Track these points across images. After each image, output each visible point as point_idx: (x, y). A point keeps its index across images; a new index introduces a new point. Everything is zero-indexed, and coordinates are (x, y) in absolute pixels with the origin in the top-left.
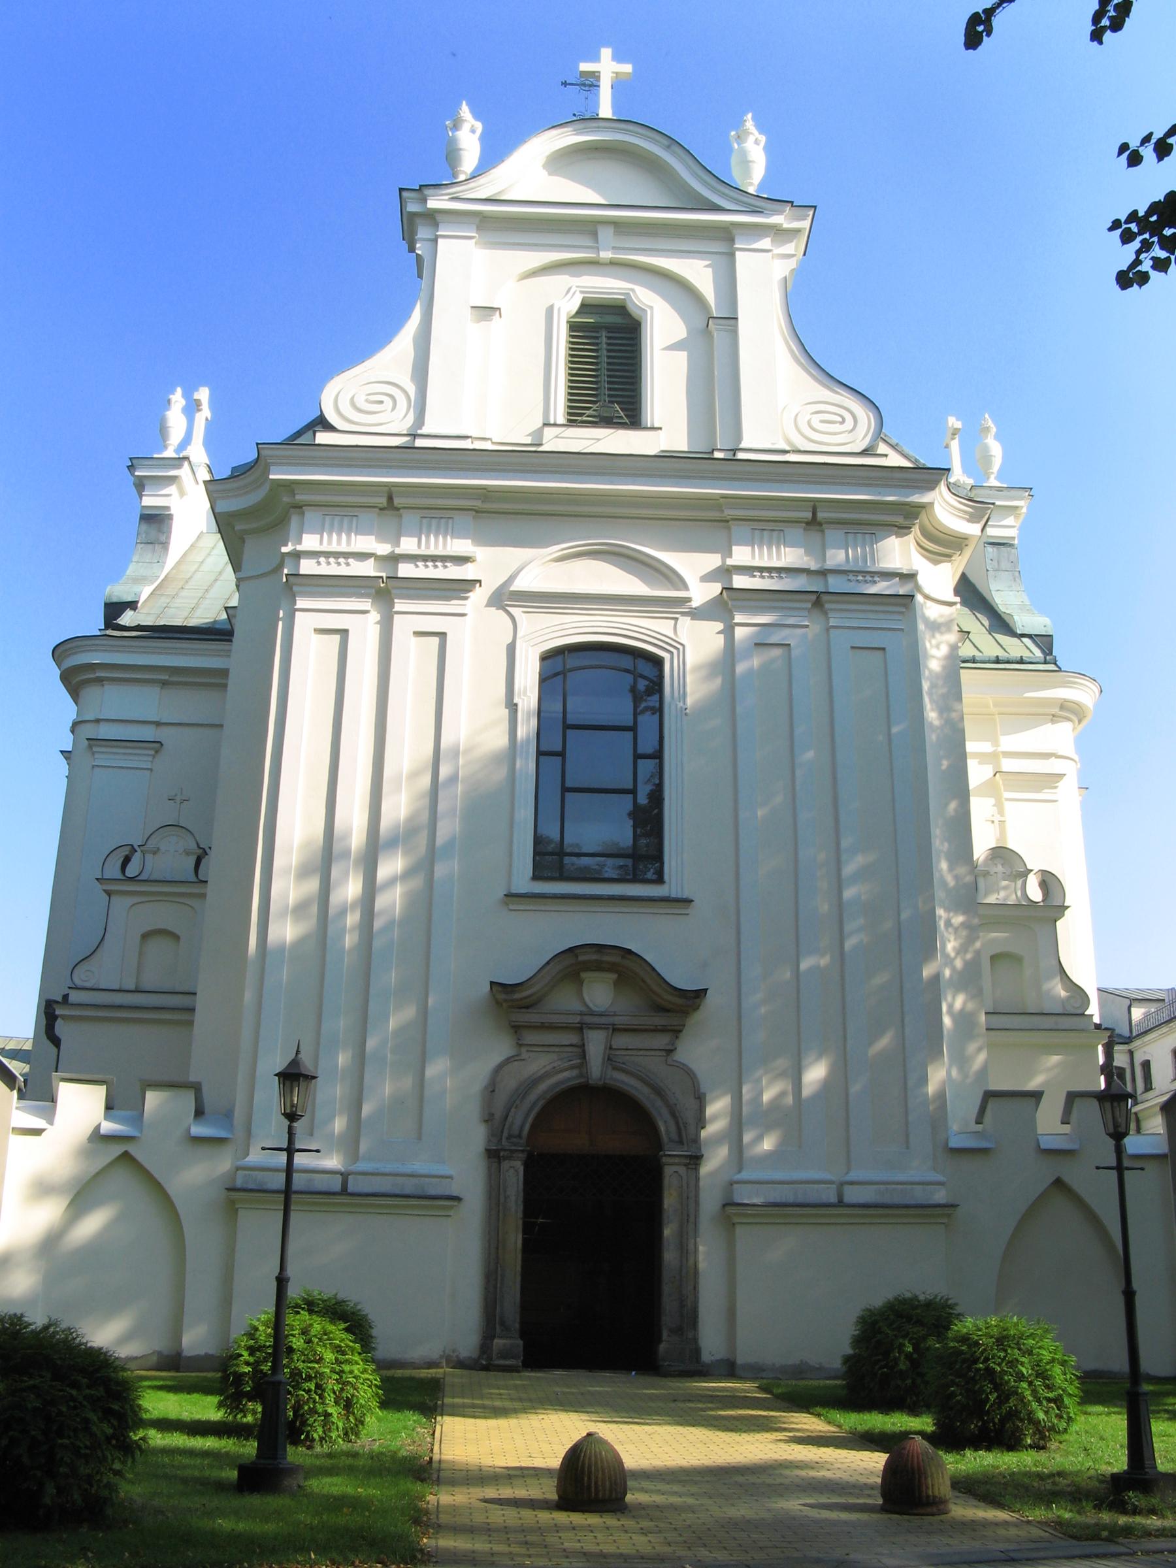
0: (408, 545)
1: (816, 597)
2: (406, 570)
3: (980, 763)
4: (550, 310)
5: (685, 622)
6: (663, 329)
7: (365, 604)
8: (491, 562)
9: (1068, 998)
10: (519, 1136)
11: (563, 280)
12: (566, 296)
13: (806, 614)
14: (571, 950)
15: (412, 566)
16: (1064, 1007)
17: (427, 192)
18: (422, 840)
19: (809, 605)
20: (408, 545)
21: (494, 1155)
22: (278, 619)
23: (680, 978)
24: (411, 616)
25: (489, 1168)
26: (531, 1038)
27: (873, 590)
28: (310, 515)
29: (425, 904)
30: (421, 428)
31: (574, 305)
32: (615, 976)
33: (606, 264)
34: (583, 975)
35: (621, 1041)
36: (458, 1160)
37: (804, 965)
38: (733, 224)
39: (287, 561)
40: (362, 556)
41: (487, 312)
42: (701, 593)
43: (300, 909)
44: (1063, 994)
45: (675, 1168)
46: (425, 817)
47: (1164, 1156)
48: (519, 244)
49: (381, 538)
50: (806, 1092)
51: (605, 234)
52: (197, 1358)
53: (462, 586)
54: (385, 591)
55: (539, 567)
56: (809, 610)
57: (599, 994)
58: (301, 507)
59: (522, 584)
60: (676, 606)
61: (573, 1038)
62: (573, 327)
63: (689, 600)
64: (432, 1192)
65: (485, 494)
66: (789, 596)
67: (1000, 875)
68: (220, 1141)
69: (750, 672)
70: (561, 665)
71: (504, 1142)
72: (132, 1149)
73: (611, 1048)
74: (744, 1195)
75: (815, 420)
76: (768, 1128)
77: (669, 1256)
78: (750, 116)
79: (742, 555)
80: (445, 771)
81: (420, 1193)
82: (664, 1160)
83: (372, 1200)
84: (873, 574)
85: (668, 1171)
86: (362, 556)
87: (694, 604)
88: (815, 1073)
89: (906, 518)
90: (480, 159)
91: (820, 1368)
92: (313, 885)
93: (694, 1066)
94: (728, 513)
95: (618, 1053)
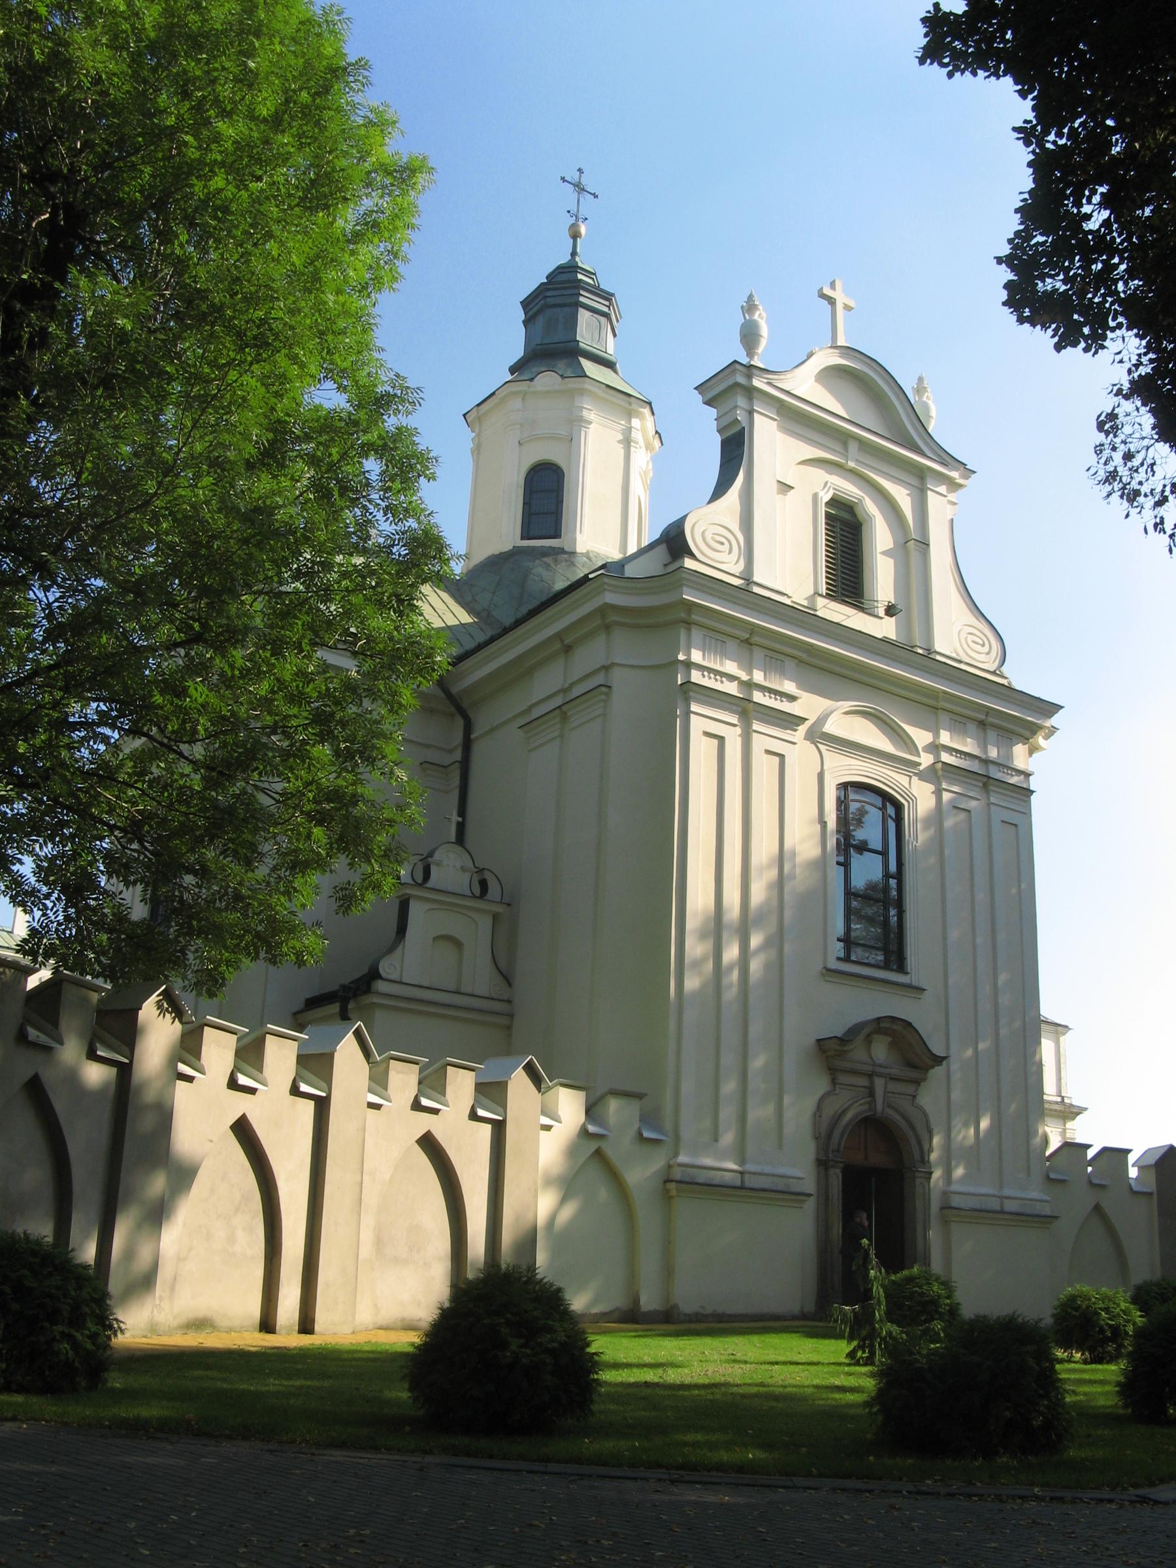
0: (758, 676)
2: (758, 697)
4: (815, 497)
6: (880, 537)
10: (838, 1150)
11: (819, 475)
15: (761, 694)
17: (755, 371)
18: (774, 920)
22: (676, 716)
24: (765, 737)
25: (819, 1173)
26: (844, 1079)
29: (777, 968)
32: (890, 1039)
36: (798, 1166)
38: (929, 468)
39: (681, 668)
41: (785, 487)
46: (775, 903)
47: (1151, 1194)
49: (740, 667)
51: (853, 447)
53: (796, 721)
55: (844, 720)
59: (830, 727)
61: (864, 1081)
65: (810, 649)
66: (970, 775)
71: (831, 1155)
74: (956, 1201)
75: (970, 638)
80: (787, 868)
83: (763, 1194)
94: (942, 704)
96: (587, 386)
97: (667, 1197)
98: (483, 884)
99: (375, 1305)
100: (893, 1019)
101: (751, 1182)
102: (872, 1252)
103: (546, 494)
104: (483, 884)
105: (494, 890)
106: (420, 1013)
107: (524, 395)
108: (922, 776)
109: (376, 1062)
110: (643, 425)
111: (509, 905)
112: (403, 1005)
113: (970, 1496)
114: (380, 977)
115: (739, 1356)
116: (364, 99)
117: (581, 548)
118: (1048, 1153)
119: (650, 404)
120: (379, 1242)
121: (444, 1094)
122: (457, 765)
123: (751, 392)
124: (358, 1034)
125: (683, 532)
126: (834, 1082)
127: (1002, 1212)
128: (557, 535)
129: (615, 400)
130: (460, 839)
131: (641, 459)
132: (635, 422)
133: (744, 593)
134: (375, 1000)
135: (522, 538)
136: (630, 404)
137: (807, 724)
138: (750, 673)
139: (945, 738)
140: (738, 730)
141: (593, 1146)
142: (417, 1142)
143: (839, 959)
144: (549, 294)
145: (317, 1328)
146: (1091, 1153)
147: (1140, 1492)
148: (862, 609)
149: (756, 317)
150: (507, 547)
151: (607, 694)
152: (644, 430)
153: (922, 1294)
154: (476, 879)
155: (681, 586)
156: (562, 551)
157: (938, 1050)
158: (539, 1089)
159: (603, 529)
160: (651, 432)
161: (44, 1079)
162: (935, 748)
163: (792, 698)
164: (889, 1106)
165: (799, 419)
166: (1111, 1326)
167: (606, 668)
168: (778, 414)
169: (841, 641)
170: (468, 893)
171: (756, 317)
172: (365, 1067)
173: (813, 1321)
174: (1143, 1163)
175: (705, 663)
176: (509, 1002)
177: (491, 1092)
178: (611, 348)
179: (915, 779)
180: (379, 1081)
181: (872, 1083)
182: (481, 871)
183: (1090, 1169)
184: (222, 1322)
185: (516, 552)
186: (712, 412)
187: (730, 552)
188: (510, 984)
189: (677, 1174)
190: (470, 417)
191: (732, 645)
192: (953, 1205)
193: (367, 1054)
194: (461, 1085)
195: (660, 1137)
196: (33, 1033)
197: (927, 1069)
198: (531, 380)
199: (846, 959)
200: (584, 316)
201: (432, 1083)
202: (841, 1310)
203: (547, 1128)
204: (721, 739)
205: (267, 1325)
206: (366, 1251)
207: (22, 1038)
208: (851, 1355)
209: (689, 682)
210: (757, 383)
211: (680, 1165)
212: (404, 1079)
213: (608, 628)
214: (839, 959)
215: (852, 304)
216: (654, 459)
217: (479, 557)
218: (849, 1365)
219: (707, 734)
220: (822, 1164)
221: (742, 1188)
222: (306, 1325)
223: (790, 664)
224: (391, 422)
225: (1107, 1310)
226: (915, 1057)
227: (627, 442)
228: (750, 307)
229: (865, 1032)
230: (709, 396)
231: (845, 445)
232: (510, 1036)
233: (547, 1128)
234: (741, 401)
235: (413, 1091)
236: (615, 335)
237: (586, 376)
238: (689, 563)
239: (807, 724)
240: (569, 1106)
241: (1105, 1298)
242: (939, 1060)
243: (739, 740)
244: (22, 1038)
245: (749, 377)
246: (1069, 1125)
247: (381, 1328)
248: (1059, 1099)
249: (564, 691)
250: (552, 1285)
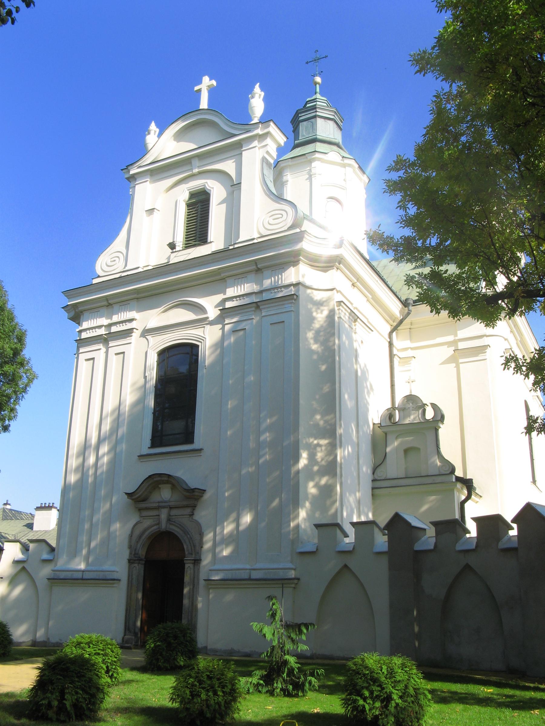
0: (115, 318)
1: (255, 305)
3: (448, 347)
5: (208, 327)
7: (101, 346)
9: (442, 466)
12: (182, 194)
13: (253, 313)
14: (150, 476)
16: (439, 471)
19: (254, 309)
20: (115, 318)
21: (130, 561)
23: (193, 484)
24: (116, 346)
26: (145, 513)
27: (280, 295)
28: (86, 314)
29: (113, 463)
30: (238, 237)
31: (186, 196)
33: (197, 175)
34: (160, 486)
35: (174, 512)
36: (118, 566)
37: (244, 472)
38: (241, 140)
40: (100, 327)
42: (212, 313)
43: (77, 470)
44: (439, 464)
45: (189, 565)
48: (176, 174)
49: (107, 318)
50: (241, 528)
51: (196, 162)
54: (104, 340)
55: (153, 317)
56: (255, 311)
57: (165, 494)
58: (224, 279)
60: (202, 322)
63: (208, 318)
64: (108, 577)
67: (411, 409)
69: (230, 344)
70: (165, 354)
72: (25, 565)
73: (170, 516)
76: (227, 545)
77: (186, 602)
78: (258, 84)
79: (231, 292)
81: (104, 578)
82: (185, 561)
84: (281, 287)
85: (187, 566)
86: (100, 327)
87: (210, 319)
88: (247, 519)
89: (294, 257)
90: (264, 110)
91: (239, 652)
92: (81, 459)
93: (200, 521)
95: (173, 517)
96: (282, 165)
119: (315, 151)
127: (250, 579)
169: (170, 273)
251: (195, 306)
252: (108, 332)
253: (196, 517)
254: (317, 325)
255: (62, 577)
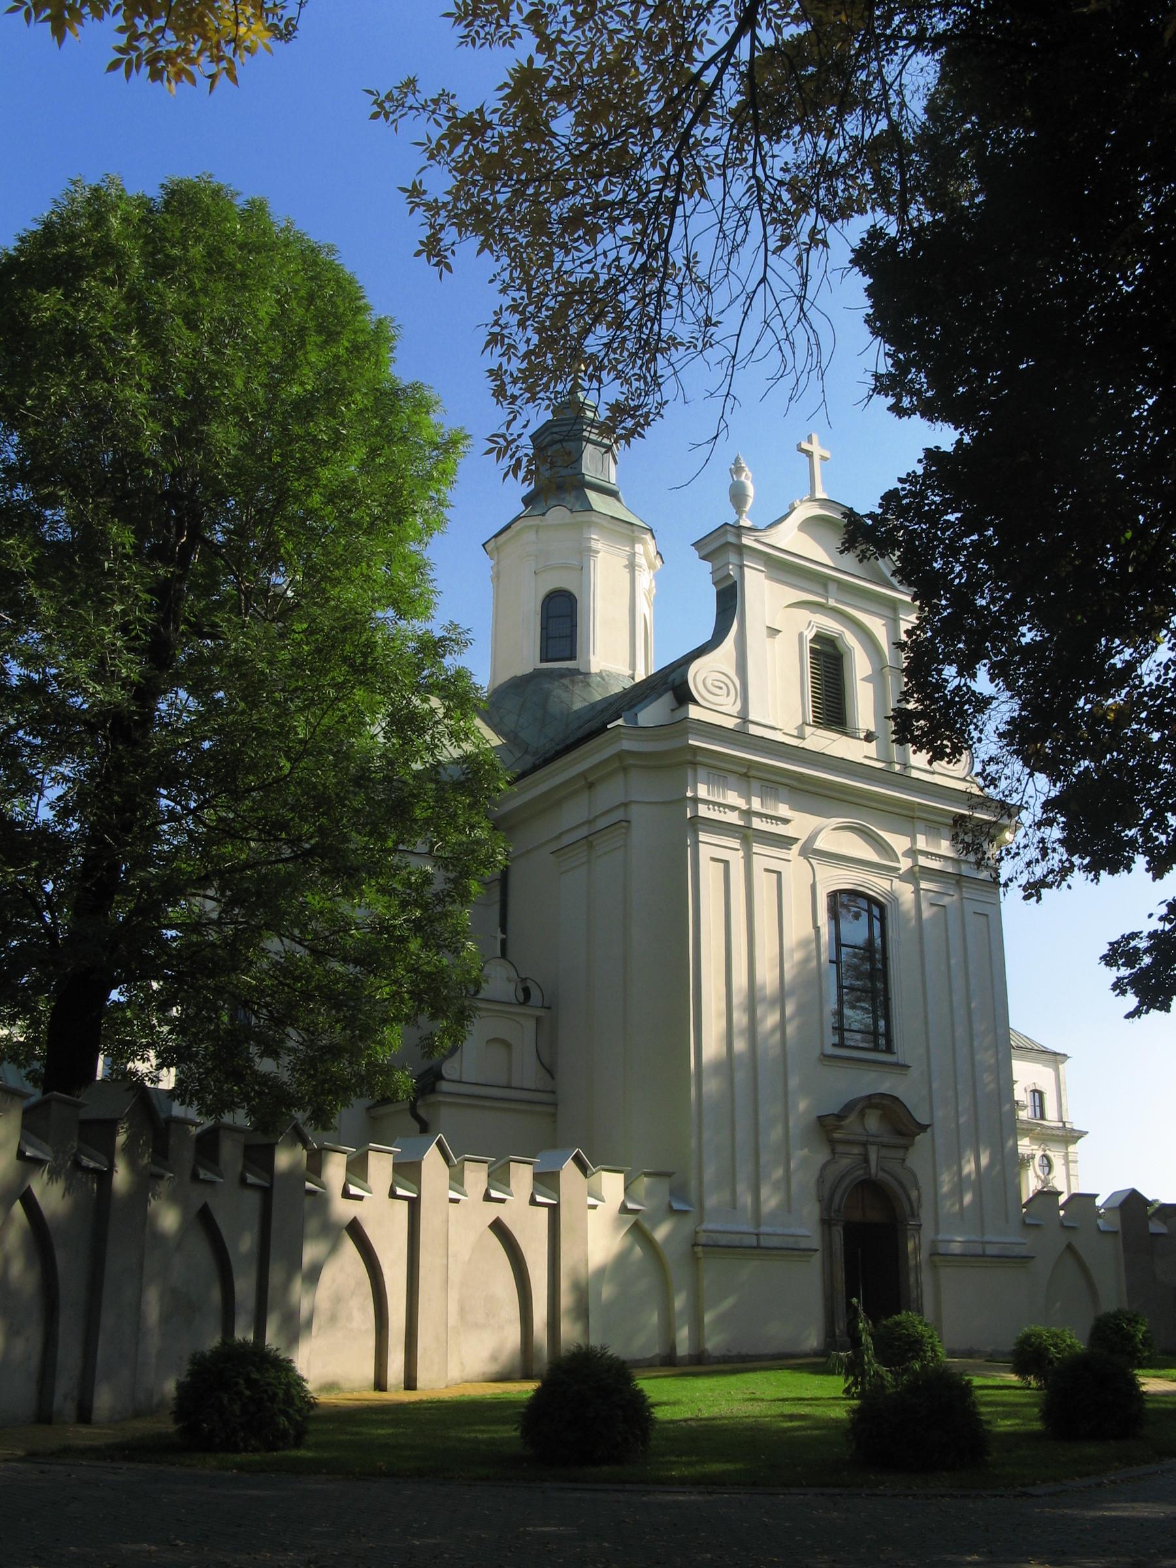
0: (756, 804)
2: (757, 823)
4: (801, 635)
7: (736, 843)
8: (802, 824)
11: (805, 615)
17: (743, 531)
26: (840, 1148)
28: (702, 772)
36: (806, 1226)
38: (901, 600)
41: (773, 632)
47: (1116, 1232)
49: (740, 796)
51: (832, 587)
52: (717, 1353)
55: (833, 834)
59: (820, 844)
62: (812, 650)
68: (686, 1212)
94: (918, 814)
96: (594, 519)
97: (695, 1259)
98: (527, 992)
99: (462, 1364)
100: (883, 1095)
101: (764, 1242)
102: (861, 1309)
103: (561, 619)
104: (527, 992)
105: (535, 992)
106: (476, 1106)
107: (538, 529)
108: (902, 878)
109: (454, 1166)
110: (646, 549)
111: (549, 1008)
112: (466, 1101)
113: (907, 1496)
114: (442, 1078)
115: (758, 1395)
116: (447, 492)
117: (594, 669)
118: (1024, 1200)
119: (651, 530)
120: (462, 1312)
121: (509, 1186)
122: (497, 883)
123: (741, 549)
124: (440, 1145)
125: (686, 682)
126: (833, 1152)
127: (984, 1255)
128: (572, 657)
129: (618, 529)
130: (504, 955)
131: (645, 580)
132: (639, 548)
133: (740, 736)
134: (441, 1098)
135: (542, 661)
136: (633, 532)
137: (800, 843)
138: (749, 802)
139: (922, 843)
140: (741, 853)
141: (631, 1218)
142: (489, 1226)
143: (834, 1045)
144: (555, 430)
145: (419, 1385)
146: (1062, 1199)
147: (1024, 1489)
148: (845, 734)
149: (743, 478)
150: (527, 669)
151: (628, 828)
152: (646, 554)
153: (909, 1335)
154: (520, 986)
155: (687, 733)
156: (576, 672)
157: (922, 1119)
158: (586, 1176)
159: (615, 654)
160: (653, 553)
161: (211, 1206)
162: (912, 853)
163: (786, 821)
164: (883, 1170)
165: (785, 569)
166: (1058, 1359)
167: (625, 805)
168: (765, 565)
170: (515, 1001)
171: (743, 478)
172: (446, 1170)
173: (818, 1364)
174: (1107, 1206)
175: (710, 798)
176: (553, 1092)
177: (546, 1180)
178: (612, 475)
179: (896, 881)
180: (457, 1180)
181: (866, 1151)
182: (524, 980)
183: (1062, 1213)
184: (346, 1385)
185: (536, 675)
186: (707, 566)
187: (728, 695)
188: (553, 1078)
189: (703, 1238)
190: (489, 547)
191: (732, 779)
192: (941, 1251)
193: (447, 1159)
194: (522, 1176)
195: (687, 1208)
196: (203, 1174)
197: (912, 1136)
198: (544, 514)
199: (841, 1044)
200: (589, 449)
201: (499, 1178)
202: (838, 1356)
203: (594, 1207)
204: (726, 863)
205: (380, 1384)
206: (453, 1320)
207: (195, 1177)
208: (847, 1391)
209: (697, 816)
210: (746, 541)
211: (705, 1231)
212: (476, 1176)
213: (625, 769)
214: (834, 1045)
215: (827, 454)
216: (656, 577)
217: (503, 678)
218: (845, 1399)
219: (713, 859)
220: (826, 1223)
221: (758, 1247)
222: (410, 1383)
223: (783, 791)
224: (450, 662)
225: (1055, 1345)
226: (901, 1124)
227: (632, 566)
228: (737, 469)
229: (859, 1107)
230: (704, 552)
231: (825, 586)
232: (555, 1122)
233: (594, 1207)
234: (733, 558)
235: (483, 1186)
236: (616, 463)
237: (593, 510)
238: (694, 712)
239: (800, 843)
240: (612, 1184)
241: (1055, 1335)
242: (923, 1128)
243: (742, 862)
244: (195, 1177)
245: (739, 536)
246: (1071, 1148)
247: (466, 1382)
248: (1061, 1125)
249: (589, 822)
250: (617, 1358)
251: (874, 839)
252: (742, 823)
253: (908, 1163)
254: (1143, 965)
255: (723, 1243)
